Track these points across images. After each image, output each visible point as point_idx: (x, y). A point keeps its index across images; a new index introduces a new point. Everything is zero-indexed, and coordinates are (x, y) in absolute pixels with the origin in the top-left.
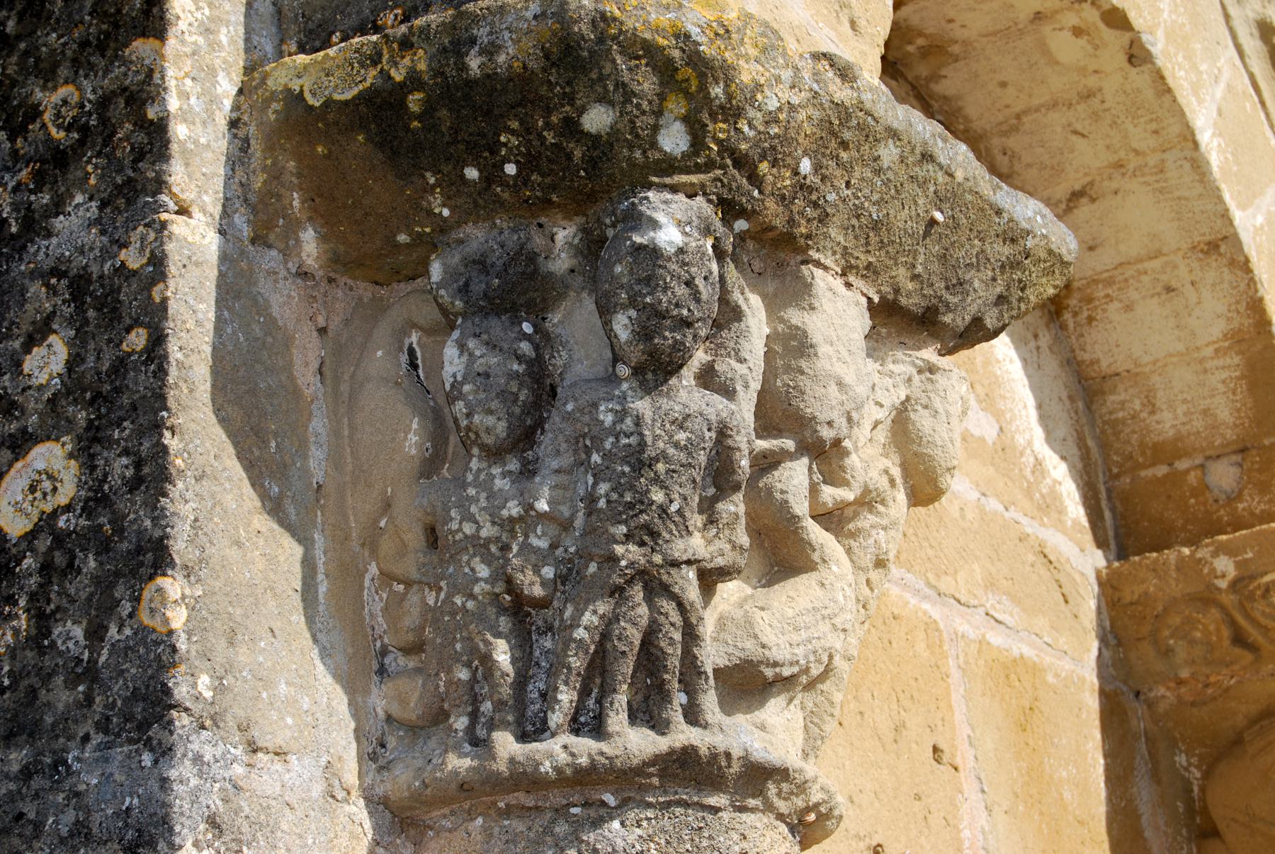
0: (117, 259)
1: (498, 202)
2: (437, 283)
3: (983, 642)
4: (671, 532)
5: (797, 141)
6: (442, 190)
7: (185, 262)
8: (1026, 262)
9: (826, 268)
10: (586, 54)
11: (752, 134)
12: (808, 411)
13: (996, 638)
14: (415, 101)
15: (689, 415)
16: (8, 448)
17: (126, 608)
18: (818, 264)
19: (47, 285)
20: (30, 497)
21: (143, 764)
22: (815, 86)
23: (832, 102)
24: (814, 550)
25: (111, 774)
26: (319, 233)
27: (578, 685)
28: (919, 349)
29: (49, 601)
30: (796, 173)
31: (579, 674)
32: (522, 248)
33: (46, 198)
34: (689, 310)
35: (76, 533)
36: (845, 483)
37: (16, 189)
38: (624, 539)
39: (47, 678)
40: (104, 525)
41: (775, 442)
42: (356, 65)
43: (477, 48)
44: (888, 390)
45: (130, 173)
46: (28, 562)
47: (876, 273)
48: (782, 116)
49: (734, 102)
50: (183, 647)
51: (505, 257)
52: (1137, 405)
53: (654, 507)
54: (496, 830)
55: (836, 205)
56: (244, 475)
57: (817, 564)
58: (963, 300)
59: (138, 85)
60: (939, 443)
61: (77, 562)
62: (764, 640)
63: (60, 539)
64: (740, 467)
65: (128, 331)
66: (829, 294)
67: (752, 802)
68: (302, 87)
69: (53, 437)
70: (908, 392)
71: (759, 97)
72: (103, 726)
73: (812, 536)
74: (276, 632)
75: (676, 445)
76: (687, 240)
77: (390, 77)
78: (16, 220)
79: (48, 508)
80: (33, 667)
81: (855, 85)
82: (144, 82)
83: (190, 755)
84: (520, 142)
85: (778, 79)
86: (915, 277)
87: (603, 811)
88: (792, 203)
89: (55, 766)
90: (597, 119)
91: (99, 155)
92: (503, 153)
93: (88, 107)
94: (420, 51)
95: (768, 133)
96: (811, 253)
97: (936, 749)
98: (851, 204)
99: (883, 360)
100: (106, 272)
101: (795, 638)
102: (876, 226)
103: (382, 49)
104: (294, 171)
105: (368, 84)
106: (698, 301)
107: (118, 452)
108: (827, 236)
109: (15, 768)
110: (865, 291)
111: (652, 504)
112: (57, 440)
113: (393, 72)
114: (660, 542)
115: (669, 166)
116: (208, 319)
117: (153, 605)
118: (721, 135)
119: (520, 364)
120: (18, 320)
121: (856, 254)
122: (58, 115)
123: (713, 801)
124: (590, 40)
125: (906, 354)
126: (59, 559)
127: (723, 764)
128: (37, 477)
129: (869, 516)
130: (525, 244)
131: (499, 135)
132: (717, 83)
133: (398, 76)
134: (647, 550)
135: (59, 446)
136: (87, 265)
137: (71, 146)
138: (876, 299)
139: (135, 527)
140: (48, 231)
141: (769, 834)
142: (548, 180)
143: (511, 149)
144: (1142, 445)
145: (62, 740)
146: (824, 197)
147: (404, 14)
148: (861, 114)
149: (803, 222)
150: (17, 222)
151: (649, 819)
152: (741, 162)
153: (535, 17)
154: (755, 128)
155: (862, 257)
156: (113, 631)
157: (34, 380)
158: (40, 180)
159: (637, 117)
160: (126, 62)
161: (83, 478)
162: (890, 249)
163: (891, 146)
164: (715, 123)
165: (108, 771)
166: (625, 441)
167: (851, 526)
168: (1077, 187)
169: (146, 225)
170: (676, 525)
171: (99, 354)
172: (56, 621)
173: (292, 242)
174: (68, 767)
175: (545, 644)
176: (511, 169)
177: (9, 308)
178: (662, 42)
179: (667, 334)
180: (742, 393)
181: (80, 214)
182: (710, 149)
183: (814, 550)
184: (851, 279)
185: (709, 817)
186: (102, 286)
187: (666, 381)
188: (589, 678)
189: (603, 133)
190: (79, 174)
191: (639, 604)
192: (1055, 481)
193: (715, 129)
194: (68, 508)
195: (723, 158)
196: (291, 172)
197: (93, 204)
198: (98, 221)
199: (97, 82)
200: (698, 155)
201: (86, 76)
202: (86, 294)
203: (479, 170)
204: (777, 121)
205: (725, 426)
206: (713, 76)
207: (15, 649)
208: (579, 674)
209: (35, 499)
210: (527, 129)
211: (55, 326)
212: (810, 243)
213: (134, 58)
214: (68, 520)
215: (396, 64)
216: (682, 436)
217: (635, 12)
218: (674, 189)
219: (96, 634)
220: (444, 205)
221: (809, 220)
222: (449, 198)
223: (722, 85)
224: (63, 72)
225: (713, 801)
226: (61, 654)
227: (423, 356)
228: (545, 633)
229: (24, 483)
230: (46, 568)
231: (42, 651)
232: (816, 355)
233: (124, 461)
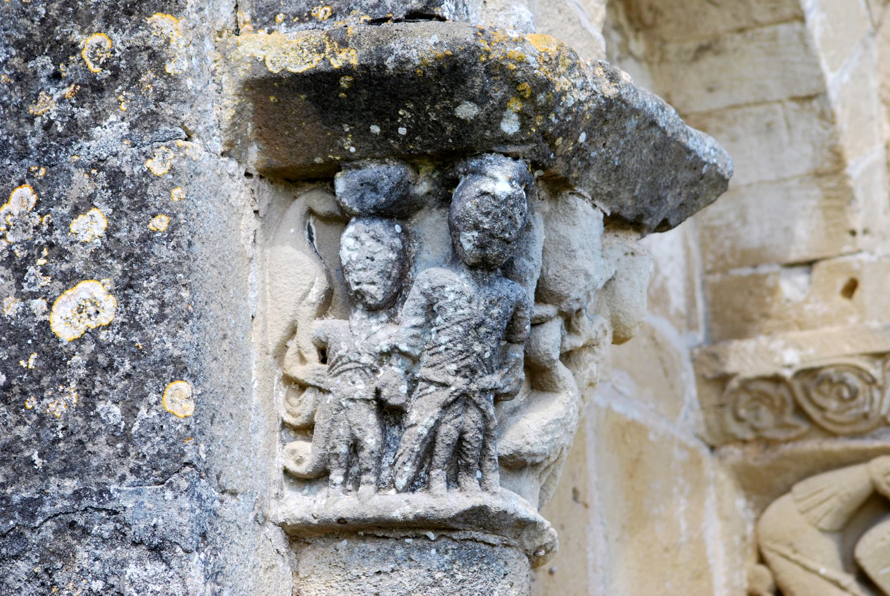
0: (145, 166)
1: (390, 149)
2: (341, 194)
3: (609, 410)
6: (353, 136)
7: (192, 174)
8: (701, 182)
9: (584, 197)
11: (556, 121)
13: (618, 407)
14: (345, 82)
16: (60, 280)
17: (153, 398)
18: (580, 195)
19: (90, 174)
20: (78, 316)
21: (166, 498)
22: (595, 87)
24: (560, 381)
25: (143, 502)
26: (261, 149)
29: (94, 387)
30: (576, 142)
32: (402, 179)
33: (87, 113)
35: (114, 344)
37: (61, 100)
38: (454, 374)
39: (93, 436)
40: (136, 342)
42: (305, 50)
43: (393, 57)
44: (605, 268)
45: (152, 107)
46: (77, 358)
47: (612, 197)
48: (574, 110)
50: (193, 427)
51: (391, 185)
52: (732, 216)
54: (357, 549)
58: (660, 209)
59: (159, 47)
61: (115, 364)
63: (101, 347)
65: (154, 216)
66: (584, 215)
68: (265, 57)
69: (95, 278)
70: (616, 268)
72: (135, 471)
73: (559, 372)
74: (234, 416)
76: (513, 190)
77: (330, 64)
78: (62, 123)
79: (93, 325)
80: (82, 428)
82: (163, 47)
84: (412, 116)
85: (574, 86)
87: (426, 542)
89: (100, 493)
90: (467, 111)
91: (128, 89)
92: (399, 121)
93: (118, 54)
94: (353, 50)
97: (575, 491)
100: (136, 173)
103: (324, 44)
104: (251, 109)
105: (313, 65)
107: (146, 296)
109: (69, 492)
110: (603, 209)
112: (99, 280)
113: (332, 61)
117: (173, 398)
119: (393, 253)
120: (65, 194)
122: (94, 54)
126: (102, 359)
128: (83, 303)
130: (404, 177)
131: (399, 110)
133: (336, 64)
134: (467, 380)
135: (101, 285)
136: (121, 166)
137: (106, 79)
138: (609, 214)
139: (160, 346)
140: (88, 135)
141: (519, 562)
142: (426, 142)
143: (405, 119)
144: (733, 249)
145: (104, 477)
147: (332, 11)
148: (619, 103)
149: (576, 170)
150: (62, 125)
153: (435, 44)
156: (143, 412)
157: (80, 237)
158: (80, 97)
160: (148, 27)
161: (120, 309)
165: (141, 500)
166: (461, 312)
168: (705, 42)
169: (166, 147)
171: (130, 228)
172: (100, 400)
173: (243, 154)
174: (110, 495)
175: (394, 433)
176: (402, 131)
177: (58, 184)
180: (529, 281)
181: (114, 129)
184: (597, 202)
186: (133, 182)
188: (424, 458)
189: (468, 119)
190: (113, 100)
192: (666, 279)
194: (109, 326)
196: (249, 110)
197: (124, 123)
198: (129, 136)
199: (124, 38)
201: (116, 31)
202: (120, 185)
203: (381, 128)
207: (67, 415)
209: (81, 317)
210: (419, 109)
211: (96, 204)
212: (577, 182)
213: (155, 27)
214: (108, 335)
215: (335, 57)
217: (498, 47)
218: (506, 155)
219: (130, 412)
220: (352, 145)
222: (357, 142)
224: (97, 24)
226: (103, 422)
227: (317, 234)
228: (394, 426)
229: (73, 305)
230: (92, 364)
231: (88, 418)
232: (575, 257)
233: (151, 302)
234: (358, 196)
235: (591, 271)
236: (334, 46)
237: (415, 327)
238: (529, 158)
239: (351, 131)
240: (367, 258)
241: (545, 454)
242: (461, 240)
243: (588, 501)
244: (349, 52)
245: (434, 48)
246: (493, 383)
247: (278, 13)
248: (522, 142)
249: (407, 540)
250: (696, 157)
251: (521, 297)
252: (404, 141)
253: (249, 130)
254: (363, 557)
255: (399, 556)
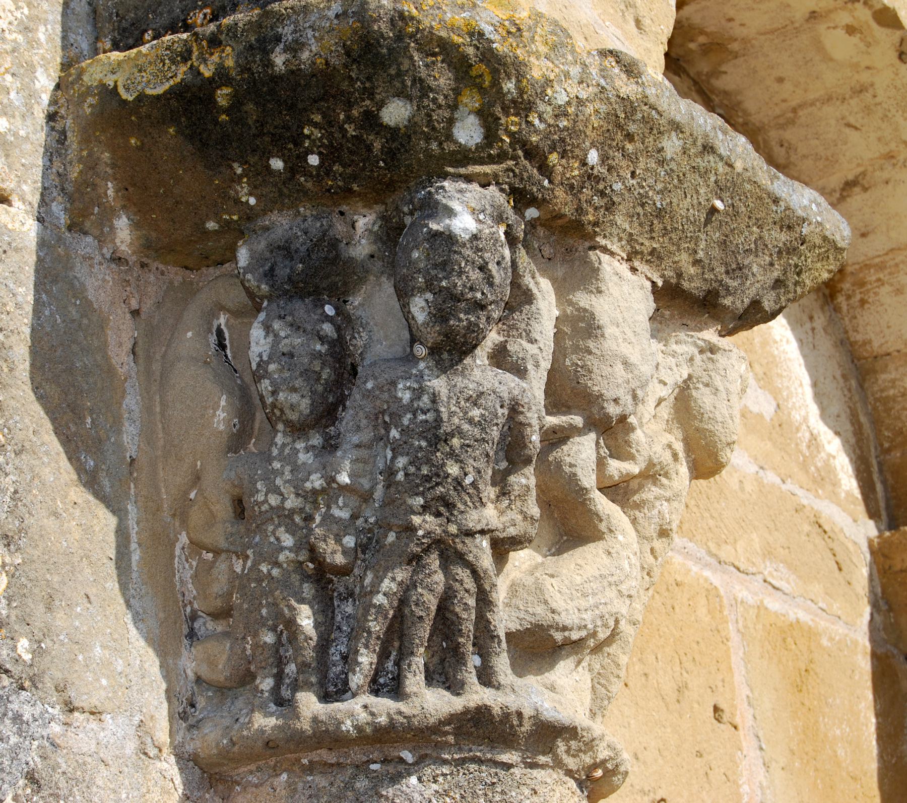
2: (243, 268)
4: (465, 504)
5: (585, 133)
8: (802, 248)
9: (612, 254)
10: (385, 51)
11: (542, 126)
12: (596, 388)
13: (774, 604)
14: (223, 96)
15: (483, 393)
18: (605, 250)
23: (618, 96)
24: (601, 521)
26: (132, 220)
27: (377, 649)
28: (701, 330)
31: (378, 638)
32: (324, 235)
34: (483, 293)
36: (631, 457)
41: (564, 418)
42: (167, 61)
49: (525, 97)
53: (449, 480)
55: (622, 194)
56: (61, 449)
57: (604, 533)
58: (743, 284)
60: (719, 419)
62: (554, 605)
64: (531, 442)
66: (615, 278)
67: (542, 759)
68: (116, 82)
70: (690, 371)
71: (549, 92)
73: (599, 507)
74: (92, 598)
75: (471, 421)
76: (480, 227)
81: (640, 81)
83: (10, 714)
84: (323, 135)
85: (567, 75)
86: (697, 262)
87: (401, 768)
88: (580, 192)
92: (307, 145)
95: (558, 126)
96: (598, 239)
97: (716, 709)
98: (636, 193)
99: (667, 341)
101: (583, 603)
102: (660, 213)
106: (491, 284)
108: (613, 223)
110: (649, 275)
111: (448, 477)
113: (202, 68)
114: (455, 513)
115: (464, 157)
116: (27, 302)
118: (512, 128)
121: (641, 240)
123: (505, 757)
124: (389, 37)
125: (688, 335)
127: (515, 723)
129: (653, 488)
130: (327, 231)
132: (509, 79)
133: (207, 72)
138: (660, 283)
142: (349, 171)
143: (314, 141)
146: (611, 186)
147: (212, 13)
151: (444, 775)
152: (533, 153)
154: (545, 121)
155: (647, 243)
159: (434, 111)
162: (673, 236)
163: (674, 138)
164: (507, 117)
167: (636, 498)
168: (850, 177)
170: (471, 497)
175: (346, 610)
178: (457, 39)
179: (462, 316)
182: (502, 141)
183: (601, 521)
184: (636, 264)
185: (501, 773)
187: (461, 360)
188: (387, 641)
189: (401, 126)
191: (436, 572)
192: (830, 456)
193: (507, 122)
195: (515, 150)
196: (106, 163)
200: (491, 147)
203: (284, 161)
204: (566, 115)
205: (517, 403)
206: (505, 72)
208: (378, 638)
210: (329, 122)
212: (597, 229)
215: (205, 61)
216: (476, 413)
217: (431, 12)
218: (468, 179)
220: (251, 194)
221: (596, 209)
222: (255, 187)
223: (513, 80)
225: (505, 757)
228: (346, 599)
232: (603, 336)
234: (267, 268)
235: (634, 358)
236: (203, 47)
237: (358, 446)
238: (506, 183)
239: (245, 174)
240: (284, 354)
241: (585, 626)
242: (412, 310)
243: (738, 720)
244: (223, 51)
245: (336, 22)
246: (484, 522)
247: (146, 31)
248: (491, 160)
249: (374, 767)
250: (788, 208)
251: (516, 393)
252: (318, 175)
253: (110, 192)
254: (310, 796)
255: (361, 790)
